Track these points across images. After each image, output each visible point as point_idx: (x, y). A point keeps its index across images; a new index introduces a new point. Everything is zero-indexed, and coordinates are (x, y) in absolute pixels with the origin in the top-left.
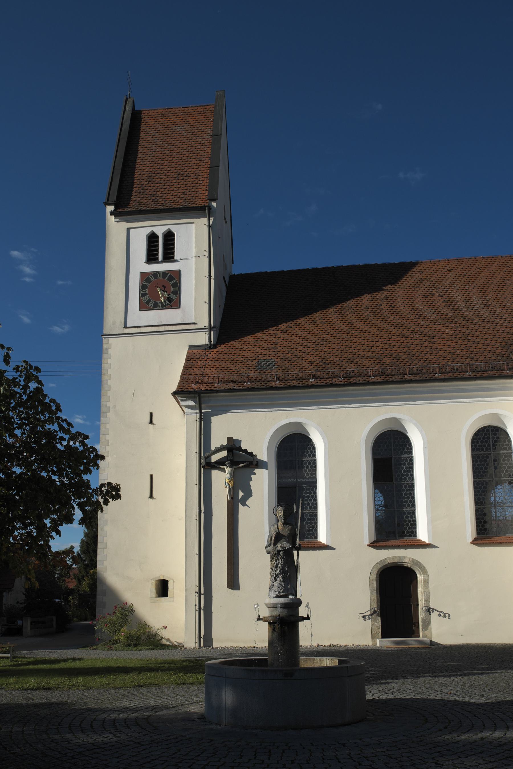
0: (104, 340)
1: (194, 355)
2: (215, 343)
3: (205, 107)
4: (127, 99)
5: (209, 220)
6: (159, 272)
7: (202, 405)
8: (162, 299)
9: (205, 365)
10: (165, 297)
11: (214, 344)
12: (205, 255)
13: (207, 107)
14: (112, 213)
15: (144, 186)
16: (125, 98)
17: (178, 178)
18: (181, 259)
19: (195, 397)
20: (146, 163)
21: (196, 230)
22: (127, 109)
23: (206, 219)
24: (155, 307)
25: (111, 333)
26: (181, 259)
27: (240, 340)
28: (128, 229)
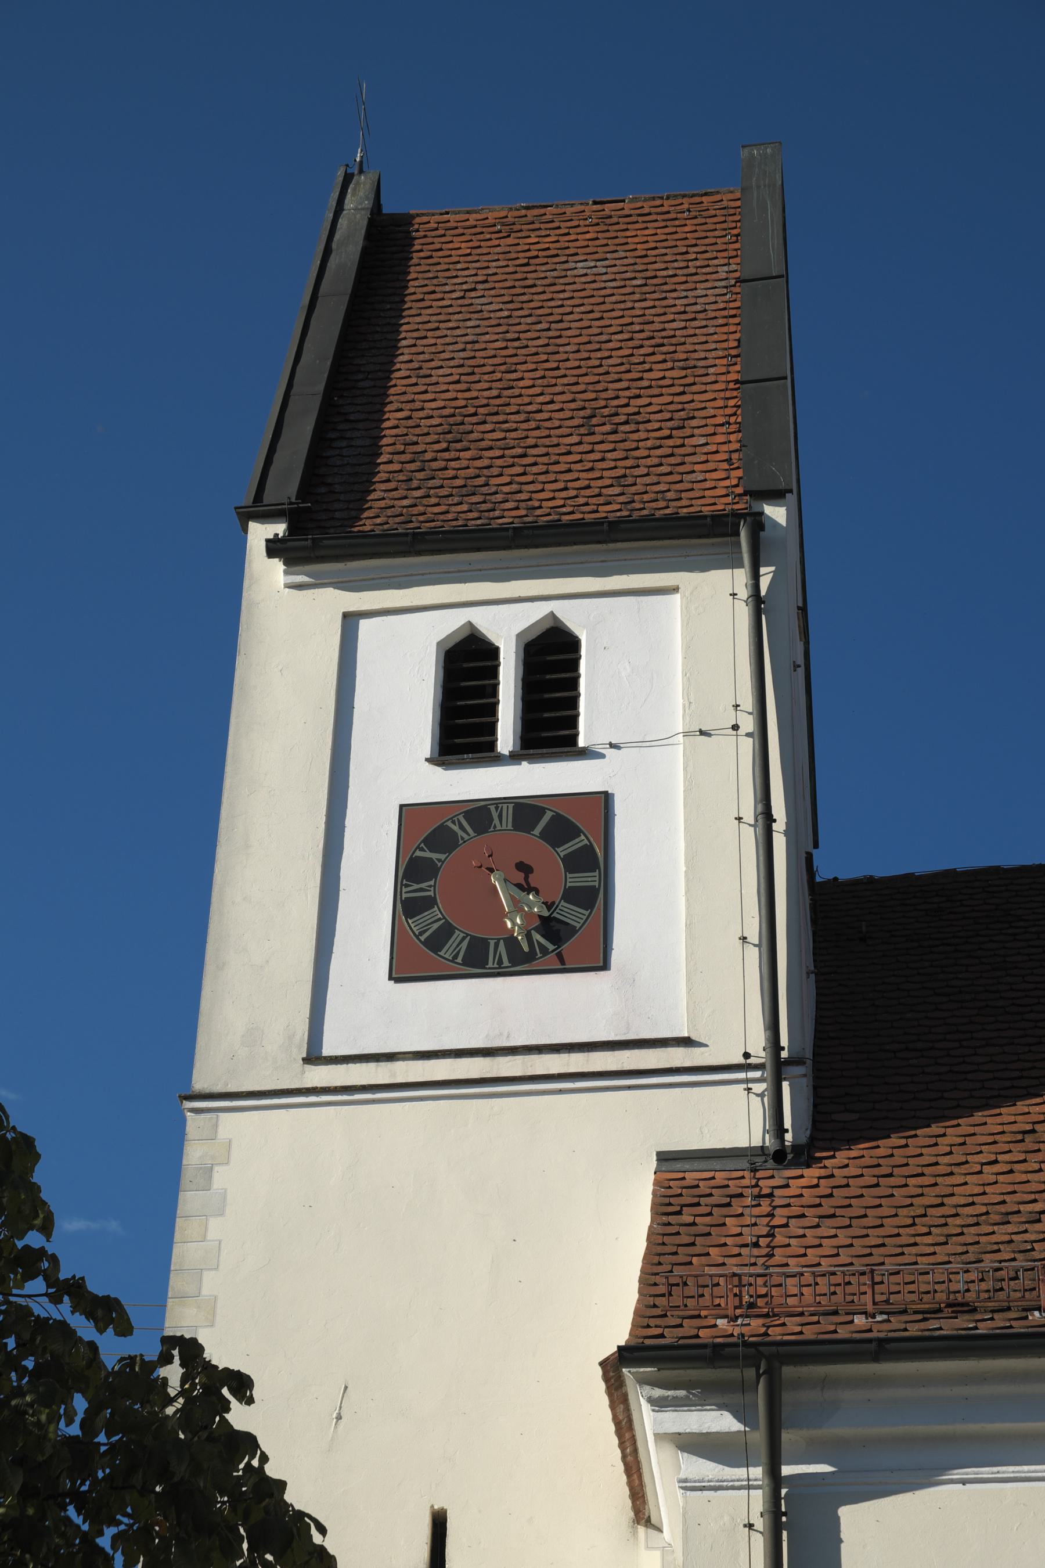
0: (194, 1124)
1: (689, 1194)
2: (803, 1140)
3: (697, 199)
4: (348, 178)
5: (756, 576)
6: (498, 802)
7: (786, 1436)
8: (514, 924)
9: (771, 1235)
10: (527, 917)
11: (795, 1147)
12: (735, 727)
13: (704, 199)
14: (273, 548)
15: (428, 456)
16: (340, 173)
17: (588, 426)
18: (612, 746)
19: (743, 1387)
20: (434, 379)
21: (686, 624)
22: (350, 203)
23: (741, 577)
24: (477, 961)
25: (232, 1088)
26: (612, 746)
27: (935, 1129)
28: (346, 616)
